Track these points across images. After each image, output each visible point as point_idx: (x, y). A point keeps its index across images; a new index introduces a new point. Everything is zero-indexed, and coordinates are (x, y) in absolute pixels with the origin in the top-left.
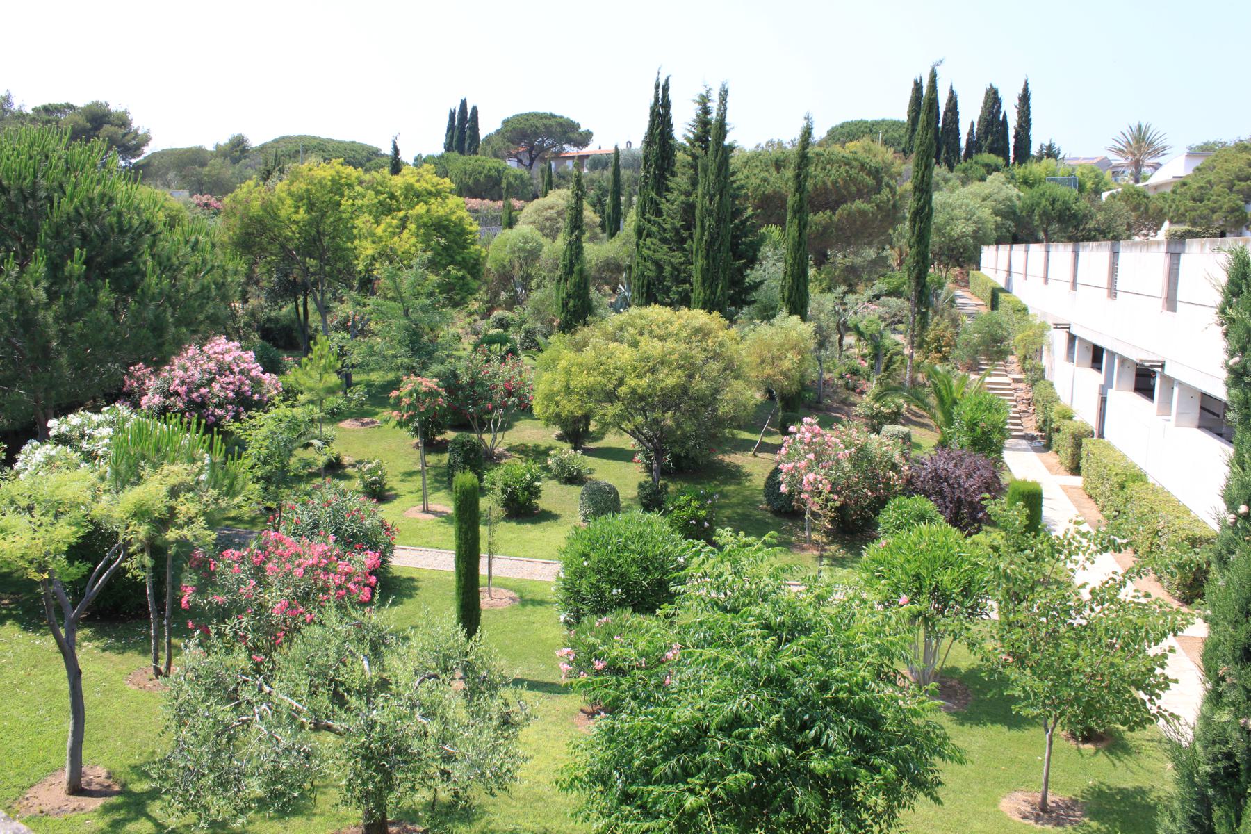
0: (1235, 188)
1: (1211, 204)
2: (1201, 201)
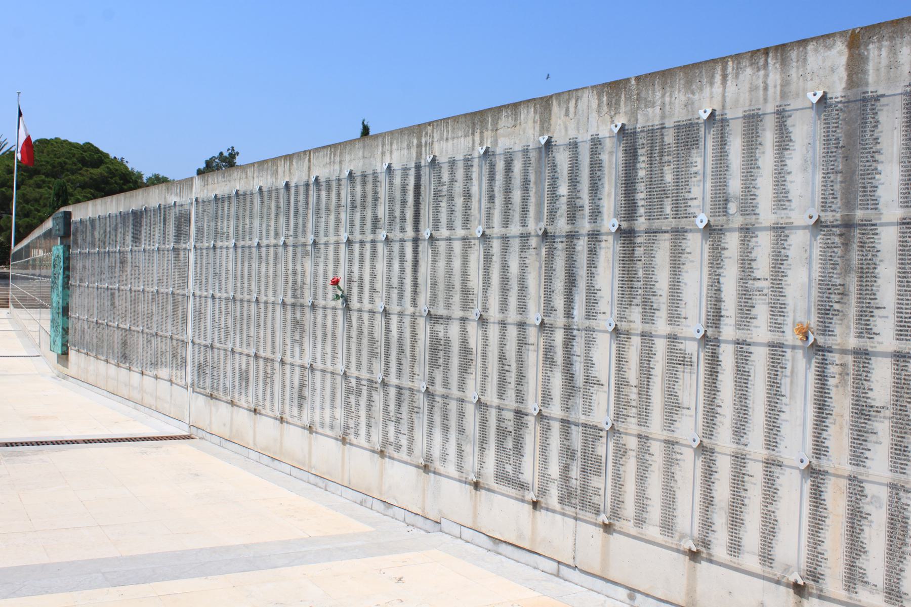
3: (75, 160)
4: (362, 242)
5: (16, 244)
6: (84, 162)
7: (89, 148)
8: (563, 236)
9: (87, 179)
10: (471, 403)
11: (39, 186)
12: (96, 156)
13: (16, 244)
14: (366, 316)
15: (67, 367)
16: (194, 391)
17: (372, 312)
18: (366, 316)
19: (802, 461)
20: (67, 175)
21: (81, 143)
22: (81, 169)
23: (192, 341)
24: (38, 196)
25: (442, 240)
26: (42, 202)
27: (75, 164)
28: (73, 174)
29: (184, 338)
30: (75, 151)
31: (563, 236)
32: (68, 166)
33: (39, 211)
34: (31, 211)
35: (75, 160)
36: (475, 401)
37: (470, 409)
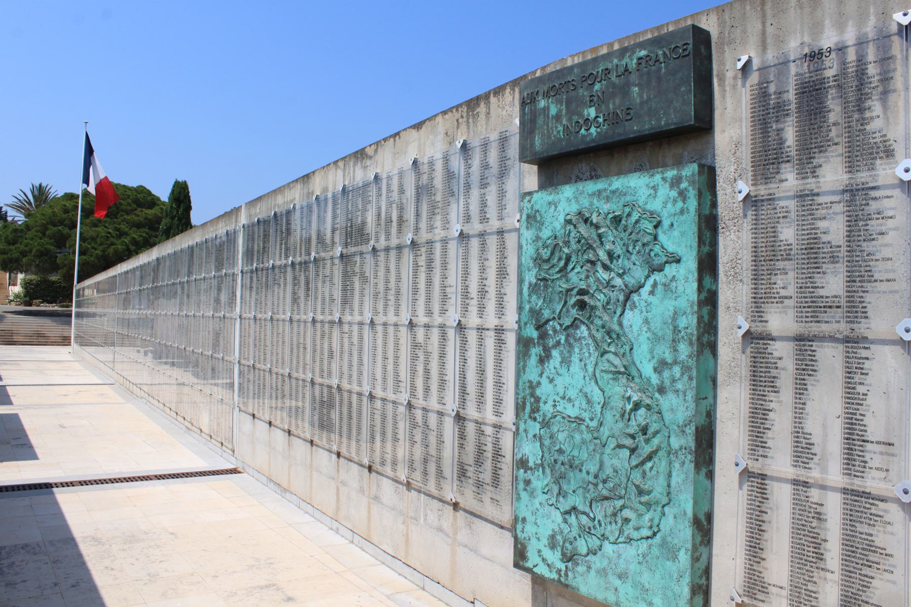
0: (47, 233)
1: (22, 247)
2: (13, 244)
3: (130, 201)
4: (481, 329)
5: (78, 282)
6: (139, 204)
7: (142, 190)
8: (833, 193)
9: (142, 219)
10: (450, 415)
11: (95, 225)
12: (149, 198)
13: (78, 282)
14: (355, 398)
15: (33, 456)
16: (240, 410)
17: (360, 394)
18: (355, 398)
19: (737, 465)
20: (122, 216)
21: (135, 186)
22: (135, 210)
23: (239, 362)
24: (94, 234)
25: (474, 236)
26: (98, 241)
27: (129, 204)
28: (128, 214)
29: (231, 359)
30: (129, 193)
31: (833, 193)
32: (124, 207)
33: (96, 249)
34: (87, 249)
35: (130, 201)
36: (454, 414)
37: (449, 423)
